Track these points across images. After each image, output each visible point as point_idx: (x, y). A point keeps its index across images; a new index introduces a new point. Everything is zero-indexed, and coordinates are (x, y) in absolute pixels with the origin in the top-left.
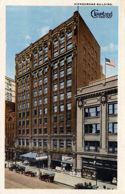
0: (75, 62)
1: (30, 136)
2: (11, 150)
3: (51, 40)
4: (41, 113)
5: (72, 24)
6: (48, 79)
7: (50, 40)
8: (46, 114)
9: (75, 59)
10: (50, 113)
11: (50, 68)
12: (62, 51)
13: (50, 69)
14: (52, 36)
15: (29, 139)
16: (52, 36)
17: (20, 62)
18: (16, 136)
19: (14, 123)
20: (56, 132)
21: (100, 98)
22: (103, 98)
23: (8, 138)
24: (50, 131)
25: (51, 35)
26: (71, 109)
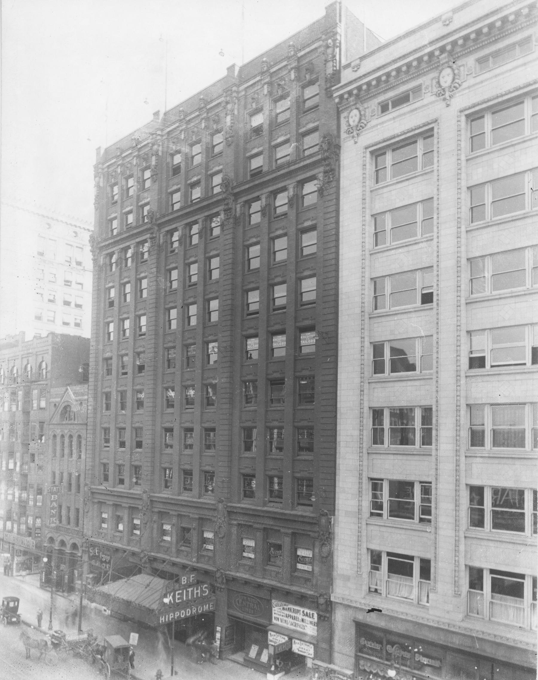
0: (329, 227)
1: (145, 496)
2: (68, 546)
3: (236, 106)
4: (194, 321)
5: (319, 50)
6: (221, 263)
7: (229, 106)
8: (215, 325)
9: (329, 198)
10: (232, 315)
11: (231, 220)
12: (281, 152)
13: (231, 226)
14: (238, 92)
15: (140, 507)
16: (238, 92)
17: (113, 181)
18: (91, 489)
19: (84, 432)
20: (249, 494)
21: (432, 79)
22: (443, 77)
23: (55, 493)
24: (232, 315)
25: (234, 89)
26: (315, 201)
